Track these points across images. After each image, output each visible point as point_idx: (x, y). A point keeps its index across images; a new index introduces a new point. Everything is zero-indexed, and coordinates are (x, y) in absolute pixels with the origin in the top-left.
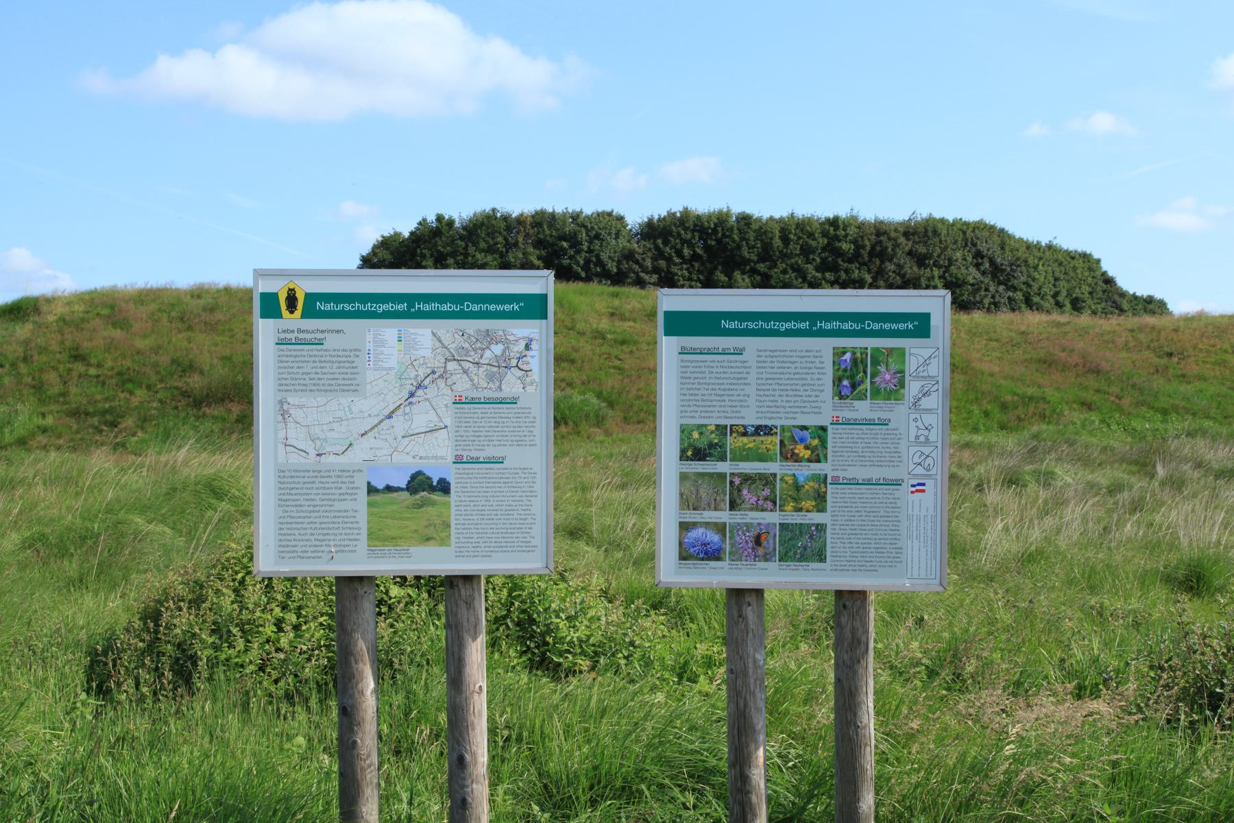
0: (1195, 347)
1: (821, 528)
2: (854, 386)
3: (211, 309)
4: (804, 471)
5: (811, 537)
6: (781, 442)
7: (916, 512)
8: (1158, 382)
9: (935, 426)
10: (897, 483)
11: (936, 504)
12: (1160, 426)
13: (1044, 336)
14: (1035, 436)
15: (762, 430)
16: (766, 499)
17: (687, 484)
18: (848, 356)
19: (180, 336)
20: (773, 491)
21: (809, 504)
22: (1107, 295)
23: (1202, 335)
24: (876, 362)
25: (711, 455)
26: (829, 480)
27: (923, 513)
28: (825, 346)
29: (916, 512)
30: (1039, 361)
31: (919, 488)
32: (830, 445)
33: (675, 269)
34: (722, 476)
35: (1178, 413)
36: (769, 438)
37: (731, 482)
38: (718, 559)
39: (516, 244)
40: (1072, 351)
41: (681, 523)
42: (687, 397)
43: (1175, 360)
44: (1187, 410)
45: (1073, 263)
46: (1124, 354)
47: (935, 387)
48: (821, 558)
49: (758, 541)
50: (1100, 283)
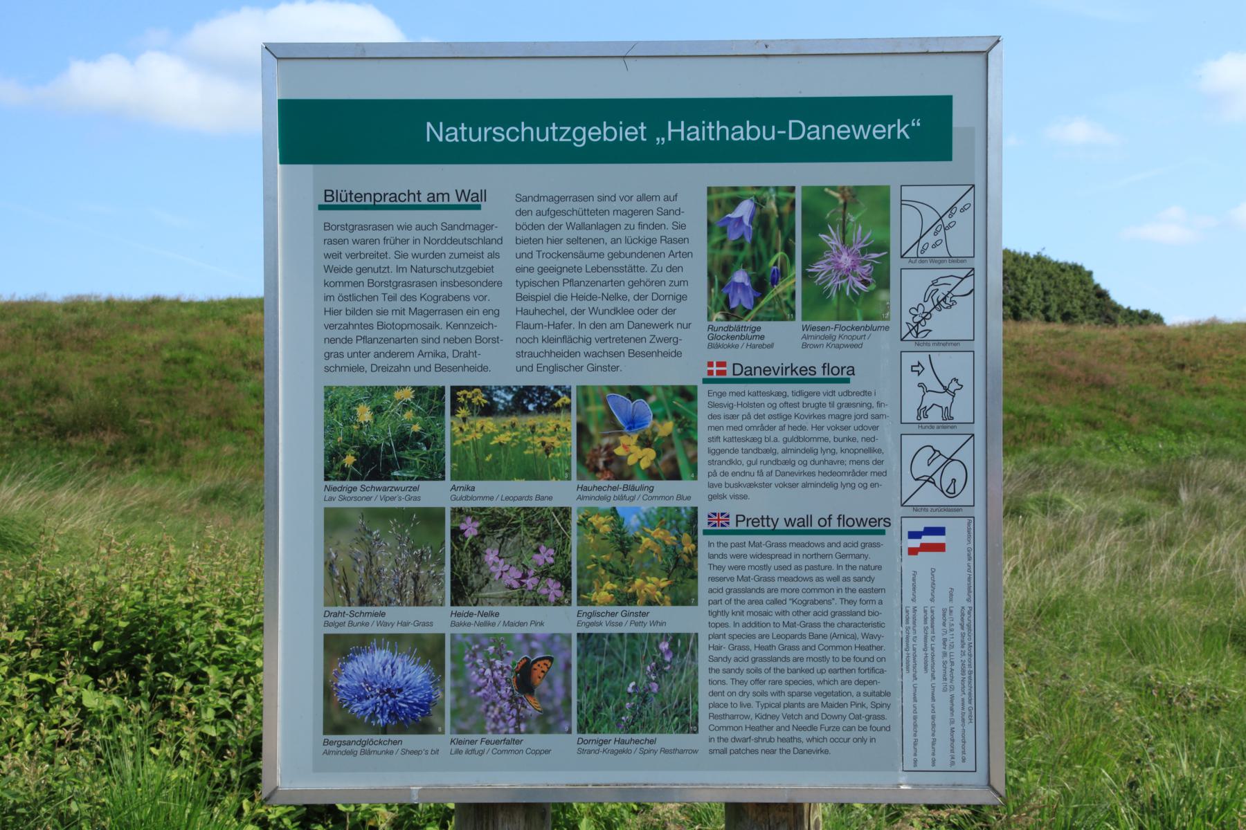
0: (1209, 358)
1: (683, 645)
2: (760, 286)
3: (86, 325)
4: (639, 502)
5: (659, 669)
6: (582, 428)
7: (923, 600)
8: (1170, 398)
9: (966, 380)
10: (875, 528)
11: (972, 579)
12: (1174, 445)
13: (1041, 347)
14: (1036, 459)
15: (530, 400)
16: (544, 574)
17: (345, 538)
18: (744, 210)
19: (46, 355)
20: (561, 552)
21: (651, 584)
22: (1101, 306)
23: (1217, 345)
24: (815, 224)
25: (403, 464)
26: (703, 524)
27: (942, 602)
28: (690, 184)
29: (923, 600)
30: (1037, 374)
31: (929, 540)
32: (702, 435)
34: (432, 517)
35: (1194, 432)
36: (551, 420)
37: (456, 532)
38: (425, 728)
40: (1073, 363)
41: (327, 637)
42: (343, 319)
43: (1187, 372)
44: (1204, 428)
45: (1064, 276)
46: (1130, 367)
47: (966, 285)
48: (688, 724)
49: (525, 680)
50: (1093, 296)
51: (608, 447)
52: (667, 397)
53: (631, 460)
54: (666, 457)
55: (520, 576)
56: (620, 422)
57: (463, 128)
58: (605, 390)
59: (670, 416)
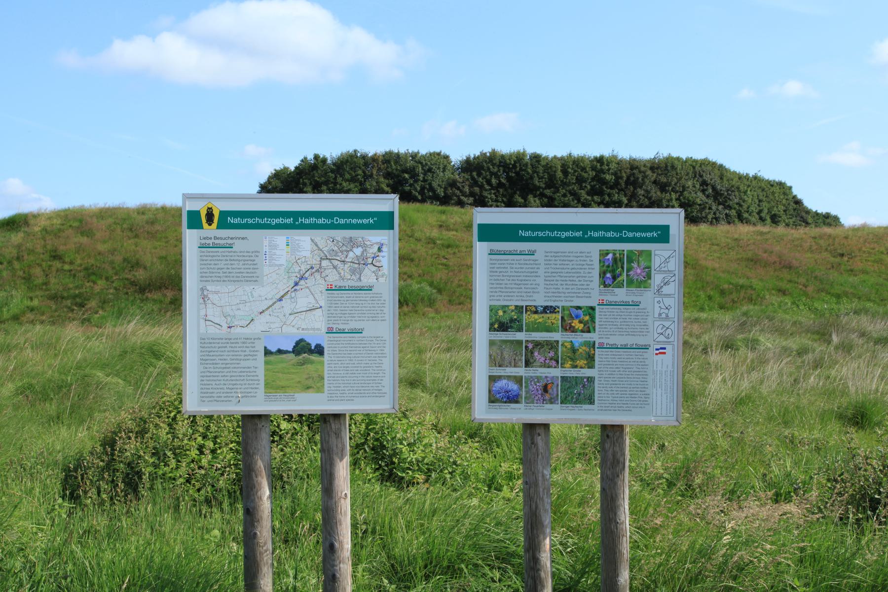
0: (860, 250)
1: (591, 380)
2: (614, 278)
3: (152, 223)
4: (579, 339)
5: (583, 386)
6: (562, 318)
7: (659, 368)
8: (834, 275)
9: (673, 306)
10: (646, 347)
11: (673, 362)
12: (835, 306)
13: (751, 241)
14: (745, 314)
15: (549, 309)
16: (551, 359)
17: (495, 348)
18: (610, 256)
19: (130, 242)
20: (556, 353)
21: (582, 362)
22: (796, 212)
23: (865, 241)
24: (630, 261)
25: (511, 327)
26: (597, 346)
27: (665, 369)
28: (594, 249)
29: (659, 368)
30: (748, 260)
31: (661, 351)
32: (597, 320)
33: (485, 194)
34: (519, 343)
35: (847, 297)
36: (554, 315)
37: (526, 347)
38: (517, 402)
39: (371, 176)
40: (772, 252)
41: (490, 376)
42: (495, 286)
43: (846, 259)
44: (854, 295)
45: (772, 189)
46: (809, 255)
47: (673, 279)
48: (591, 401)
49: (545, 389)
50: (792, 203)
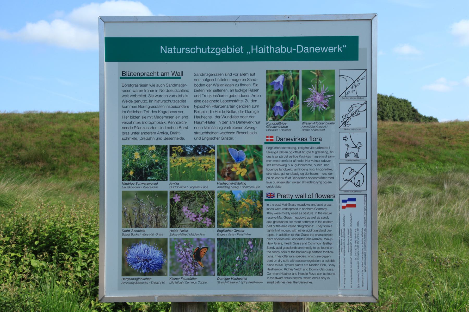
0: (455, 134)
1: (257, 242)
2: (286, 108)
3: (32, 122)
4: (240, 189)
5: (248, 251)
6: (219, 161)
7: (347, 226)
8: (441, 150)
9: (363, 143)
10: (329, 198)
11: (366, 218)
12: (442, 167)
13: (392, 130)
14: (390, 173)
15: (199, 150)
16: (205, 216)
17: (130, 202)
18: (280, 79)
19: (17, 133)
20: (211, 208)
21: (245, 220)
22: (414, 115)
23: (458, 130)
24: (307, 84)
25: (152, 174)
26: (264, 197)
27: (354, 226)
28: (260, 69)
29: (347, 226)
30: (390, 141)
31: (350, 203)
32: (264, 164)
34: (163, 194)
35: (449, 162)
36: (207, 158)
37: (172, 200)
38: (160, 274)
40: (404, 136)
41: (123, 240)
42: (129, 120)
43: (447, 140)
44: (453, 161)
45: (400, 104)
46: (425, 138)
47: (364, 107)
48: (259, 272)
49: (197, 256)
50: (411, 111)
51: (229, 168)
52: (251, 149)
53: (238, 173)
54: (251, 172)
55: (196, 216)
56: (234, 159)
57: (174, 48)
58: (228, 146)
59: (252, 156)
